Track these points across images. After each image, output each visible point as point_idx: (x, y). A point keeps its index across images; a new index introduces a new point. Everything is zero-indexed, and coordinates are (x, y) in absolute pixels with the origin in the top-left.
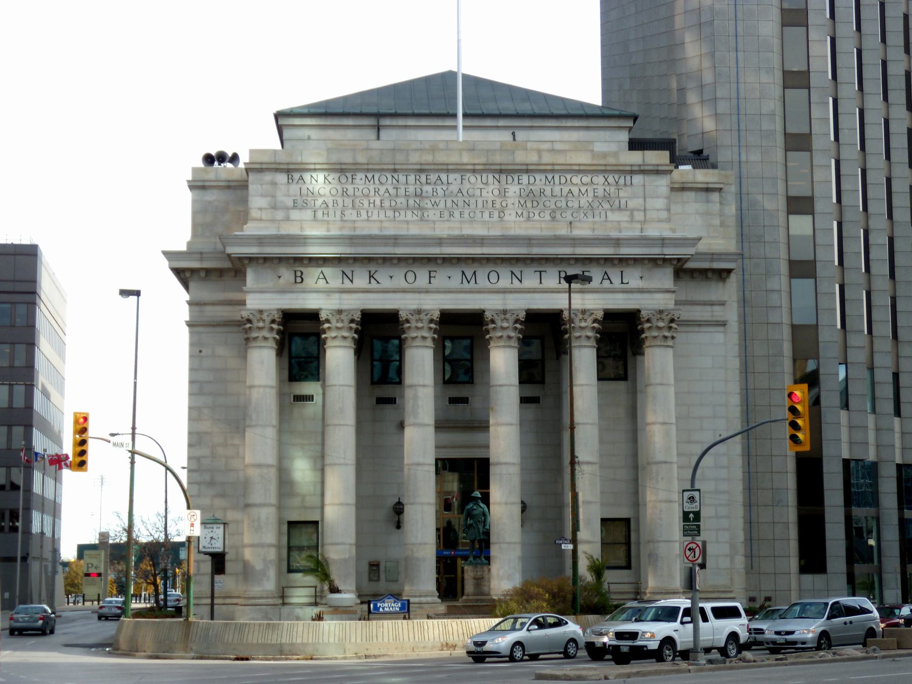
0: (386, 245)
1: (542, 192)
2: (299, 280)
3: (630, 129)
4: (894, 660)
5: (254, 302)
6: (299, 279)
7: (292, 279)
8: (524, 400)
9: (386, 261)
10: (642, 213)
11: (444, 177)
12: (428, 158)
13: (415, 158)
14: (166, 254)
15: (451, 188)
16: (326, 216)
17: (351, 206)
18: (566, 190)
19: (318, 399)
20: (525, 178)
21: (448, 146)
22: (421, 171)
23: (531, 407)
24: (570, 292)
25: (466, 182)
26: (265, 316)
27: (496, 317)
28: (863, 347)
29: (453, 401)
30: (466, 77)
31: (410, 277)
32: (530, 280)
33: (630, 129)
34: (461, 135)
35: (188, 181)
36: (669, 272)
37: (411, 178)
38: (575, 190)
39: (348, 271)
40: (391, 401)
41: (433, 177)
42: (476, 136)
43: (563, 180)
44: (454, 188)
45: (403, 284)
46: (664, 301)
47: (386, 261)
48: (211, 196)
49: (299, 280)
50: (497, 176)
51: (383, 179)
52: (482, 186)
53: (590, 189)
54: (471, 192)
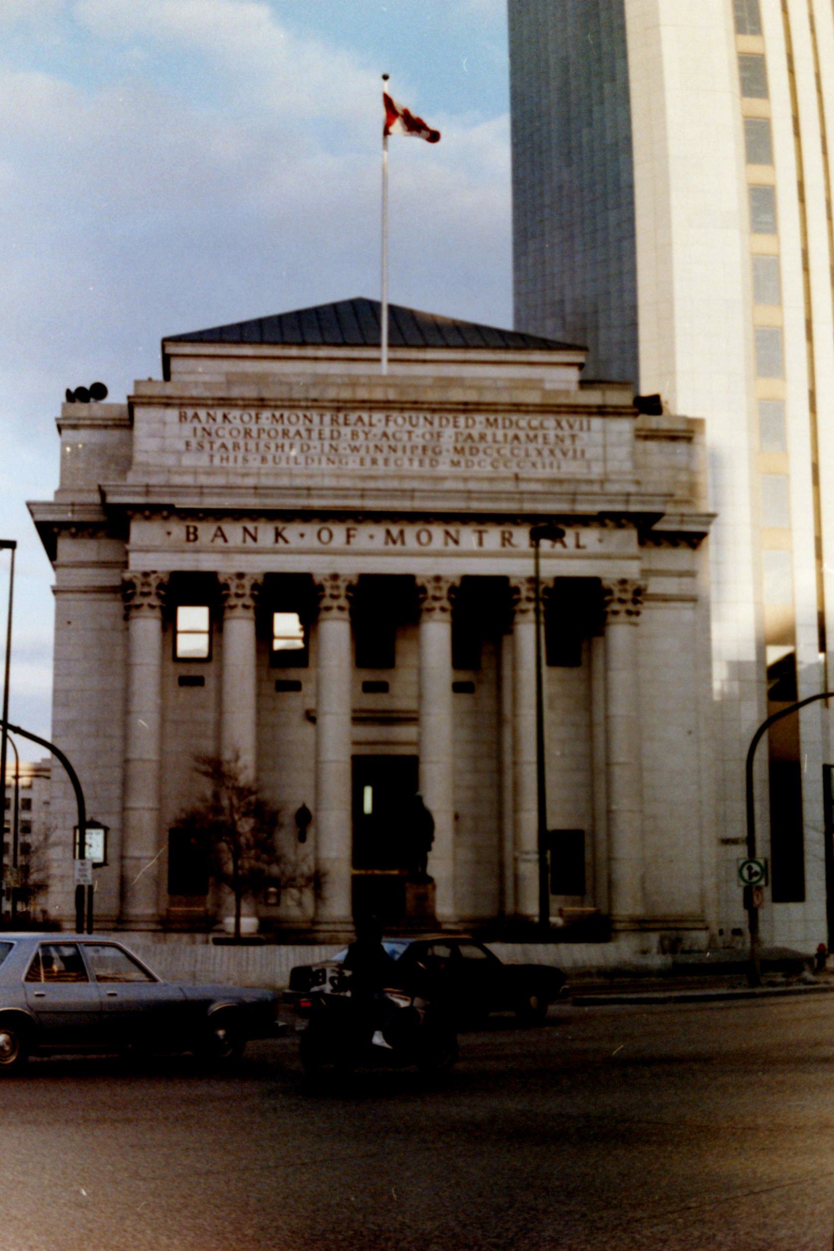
0: (298, 496)
1: (482, 437)
2: (192, 537)
3: (581, 366)
4: (573, 497)
5: (138, 563)
6: (192, 536)
7: (183, 535)
8: (458, 687)
9: (306, 515)
10: (601, 464)
11: (365, 416)
12: (346, 394)
13: (332, 393)
14: (29, 505)
15: (374, 430)
16: (224, 462)
17: (254, 450)
18: (511, 433)
19: (210, 682)
20: (462, 419)
21: (372, 382)
22: (339, 409)
23: (465, 698)
24: (537, 556)
25: (391, 424)
26: (152, 579)
27: (229, 582)
28: (348, 530)
29: (369, 687)
30: (392, 309)
31: (325, 535)
32: (468, 536)
33: (581, 366)
34: (385, 368)
35: (57, 419)
36: (631, 535)
37: (327, 418)
38: (522, 435)
39: (250, 526)
40: (296, 686)
41: (353, 417)
42: (401, 370)
43: (507, 423)
44: (378, 430)
45: (316, 544)
46: (631, 570)
47: (306, 515)
48: (83, 437)
49: (192, 537)
50: (429, 416)
51: (293, 419)
52: (410, 428)
53: (540, 433)
54: (398, 435)
